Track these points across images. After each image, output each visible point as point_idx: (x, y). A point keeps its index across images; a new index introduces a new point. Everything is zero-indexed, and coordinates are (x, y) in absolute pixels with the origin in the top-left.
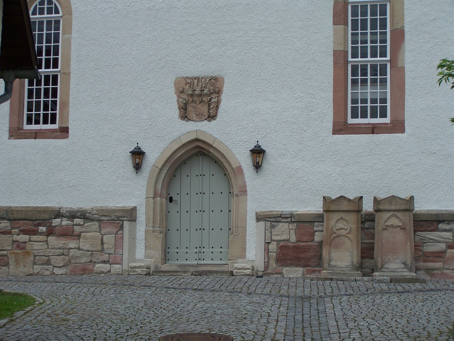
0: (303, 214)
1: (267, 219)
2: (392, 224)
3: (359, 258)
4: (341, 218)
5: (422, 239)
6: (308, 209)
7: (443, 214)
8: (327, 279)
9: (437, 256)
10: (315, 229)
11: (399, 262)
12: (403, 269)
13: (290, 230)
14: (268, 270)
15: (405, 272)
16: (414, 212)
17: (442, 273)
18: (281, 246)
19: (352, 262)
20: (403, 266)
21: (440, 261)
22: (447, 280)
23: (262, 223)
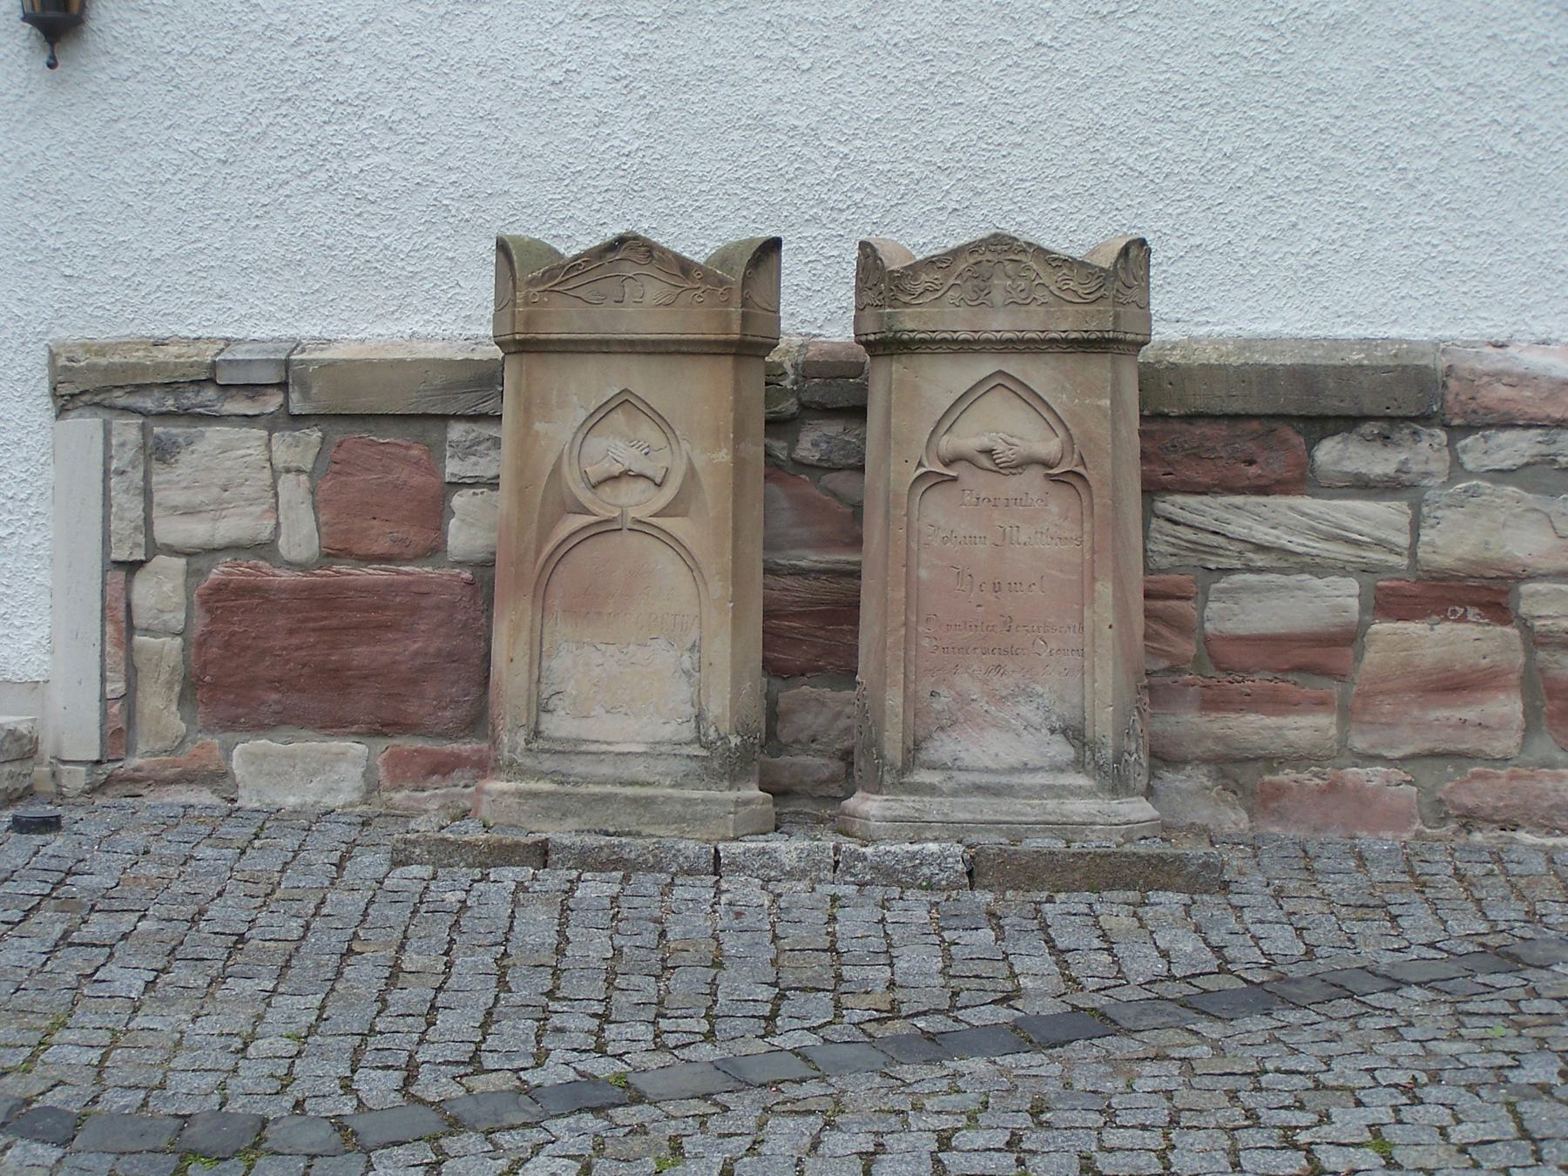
0: (369, 363)
1: (122, 399)
2: (985, 441)
3: (755, 680)
4: (625, 401)
5: (1195, 547)
6: (411, 324)
7: (1345, 373)
8: (504, 854)
9: (1300, 669)
10: (453, 468)
11: (1037, 719)
12: (1061, 770)
13: (275, 475)
14: (130, 749)
15: (1075, 792)
16: (1147, 354)
17: (1333, 787)
18: (219, 589)
19: (699, 717)
20: (1062, 750)
21: (1322, 703)
22: (1365, 838)
23: (86, 426)
